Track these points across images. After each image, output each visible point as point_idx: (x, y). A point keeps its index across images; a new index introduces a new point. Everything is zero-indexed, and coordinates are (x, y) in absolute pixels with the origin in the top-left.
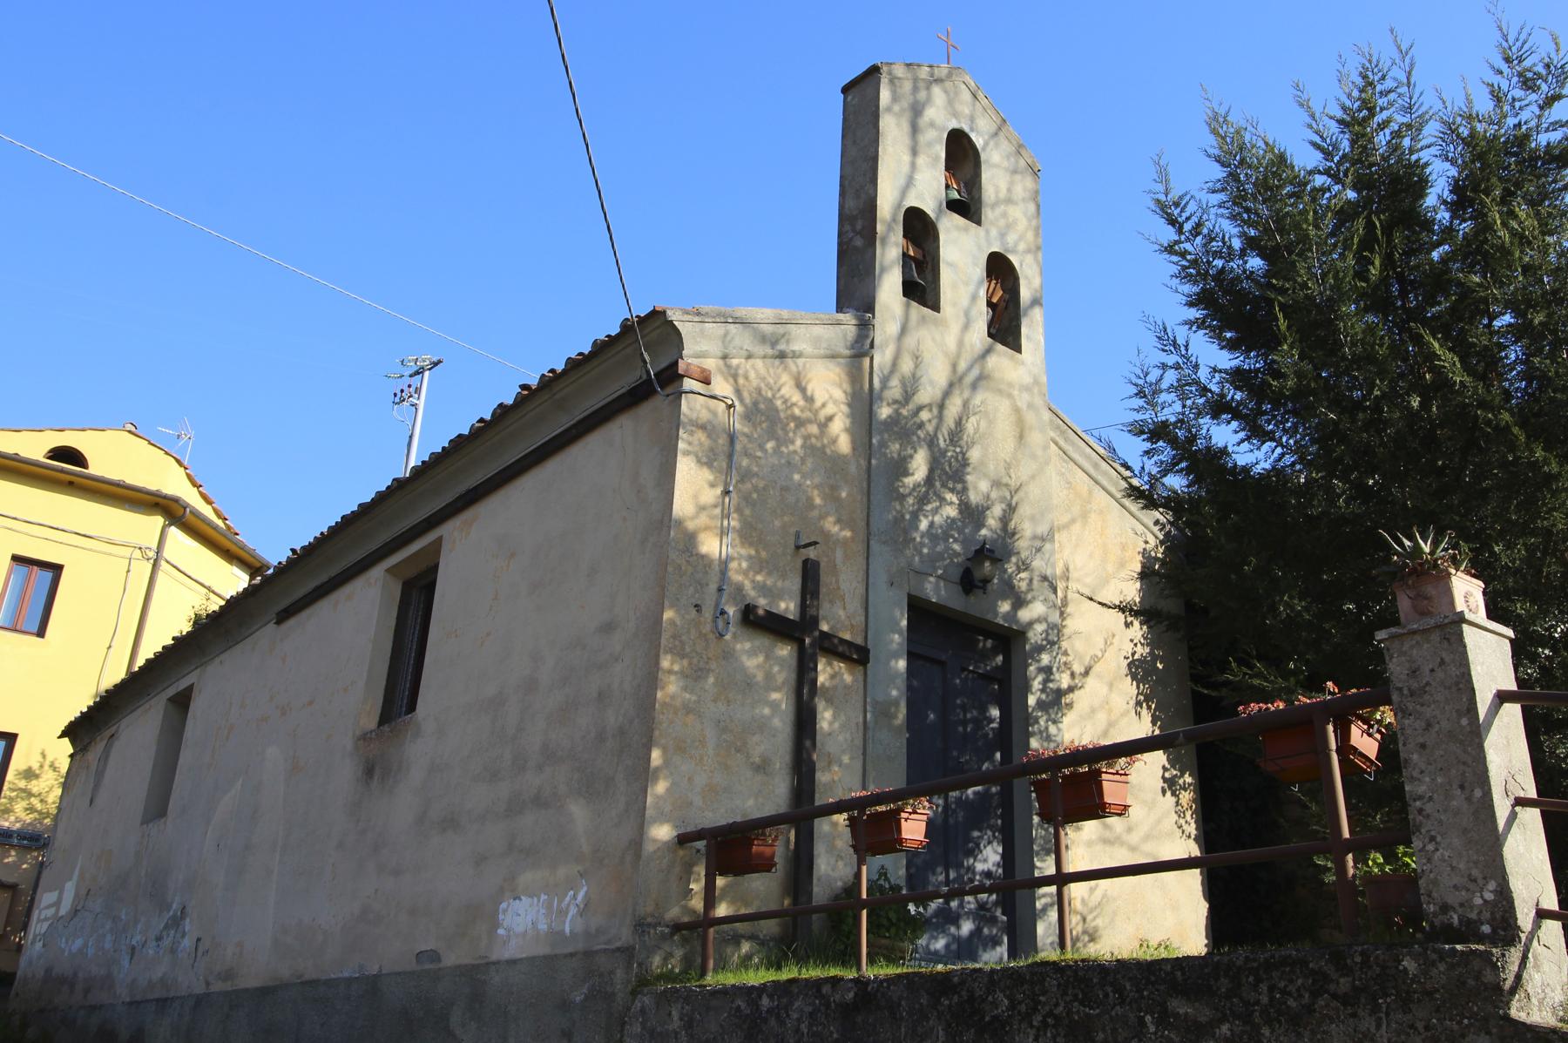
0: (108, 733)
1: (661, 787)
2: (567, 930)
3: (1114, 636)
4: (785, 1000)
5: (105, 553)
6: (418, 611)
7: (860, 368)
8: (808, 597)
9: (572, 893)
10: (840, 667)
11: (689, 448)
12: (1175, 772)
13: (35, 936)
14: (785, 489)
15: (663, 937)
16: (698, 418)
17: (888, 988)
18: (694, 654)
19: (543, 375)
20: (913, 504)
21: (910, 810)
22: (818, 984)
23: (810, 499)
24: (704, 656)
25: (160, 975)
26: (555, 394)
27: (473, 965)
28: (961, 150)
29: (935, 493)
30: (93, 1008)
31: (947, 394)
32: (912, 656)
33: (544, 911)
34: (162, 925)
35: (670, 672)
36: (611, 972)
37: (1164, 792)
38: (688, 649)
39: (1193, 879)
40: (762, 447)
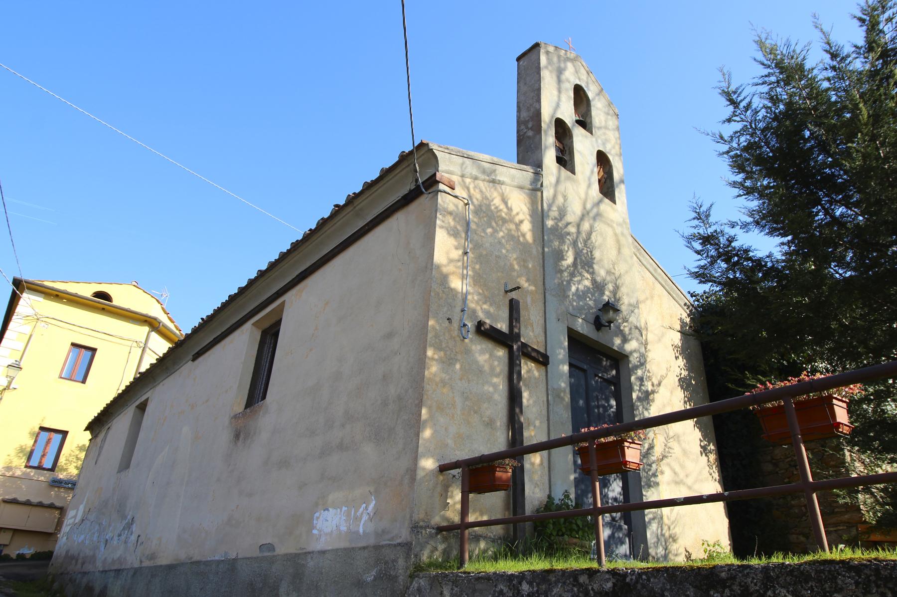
0: (107, 427)
1: (427, 433)
2: (361, 531)
3: (670, 367)
4: (544, 587)
5: (119, 344)
6: (269, 349)
7: (536, 197)
8: (514, 321)
9: (364, 505)
10: (532, 366)
11: (443, 224)
12: (706, 443)
13: (64, 534)
14: (498, 257)
15: (431, 536)
16: (447, 208)
17: (649, 580)
18: (448, 349)
19: (349, 195)
20: (567, 277)
21: (631, 441)
22: (575, 575)
23: (512, 265)
24: (454, 351)
25: (118, 556)
26: (355, 207)
27: (296, 554)
28: (580, 96)
29: (578, 272)
30: (85, 573)
31: (582, 218)
32: (571, 365)
33: (345, 518)
34: (122, 528)
35: (433, 359)
36: (395, 561)
37: (701, 454)
38: (444, 345)
39: (719, 507)
40: (484, 231)
